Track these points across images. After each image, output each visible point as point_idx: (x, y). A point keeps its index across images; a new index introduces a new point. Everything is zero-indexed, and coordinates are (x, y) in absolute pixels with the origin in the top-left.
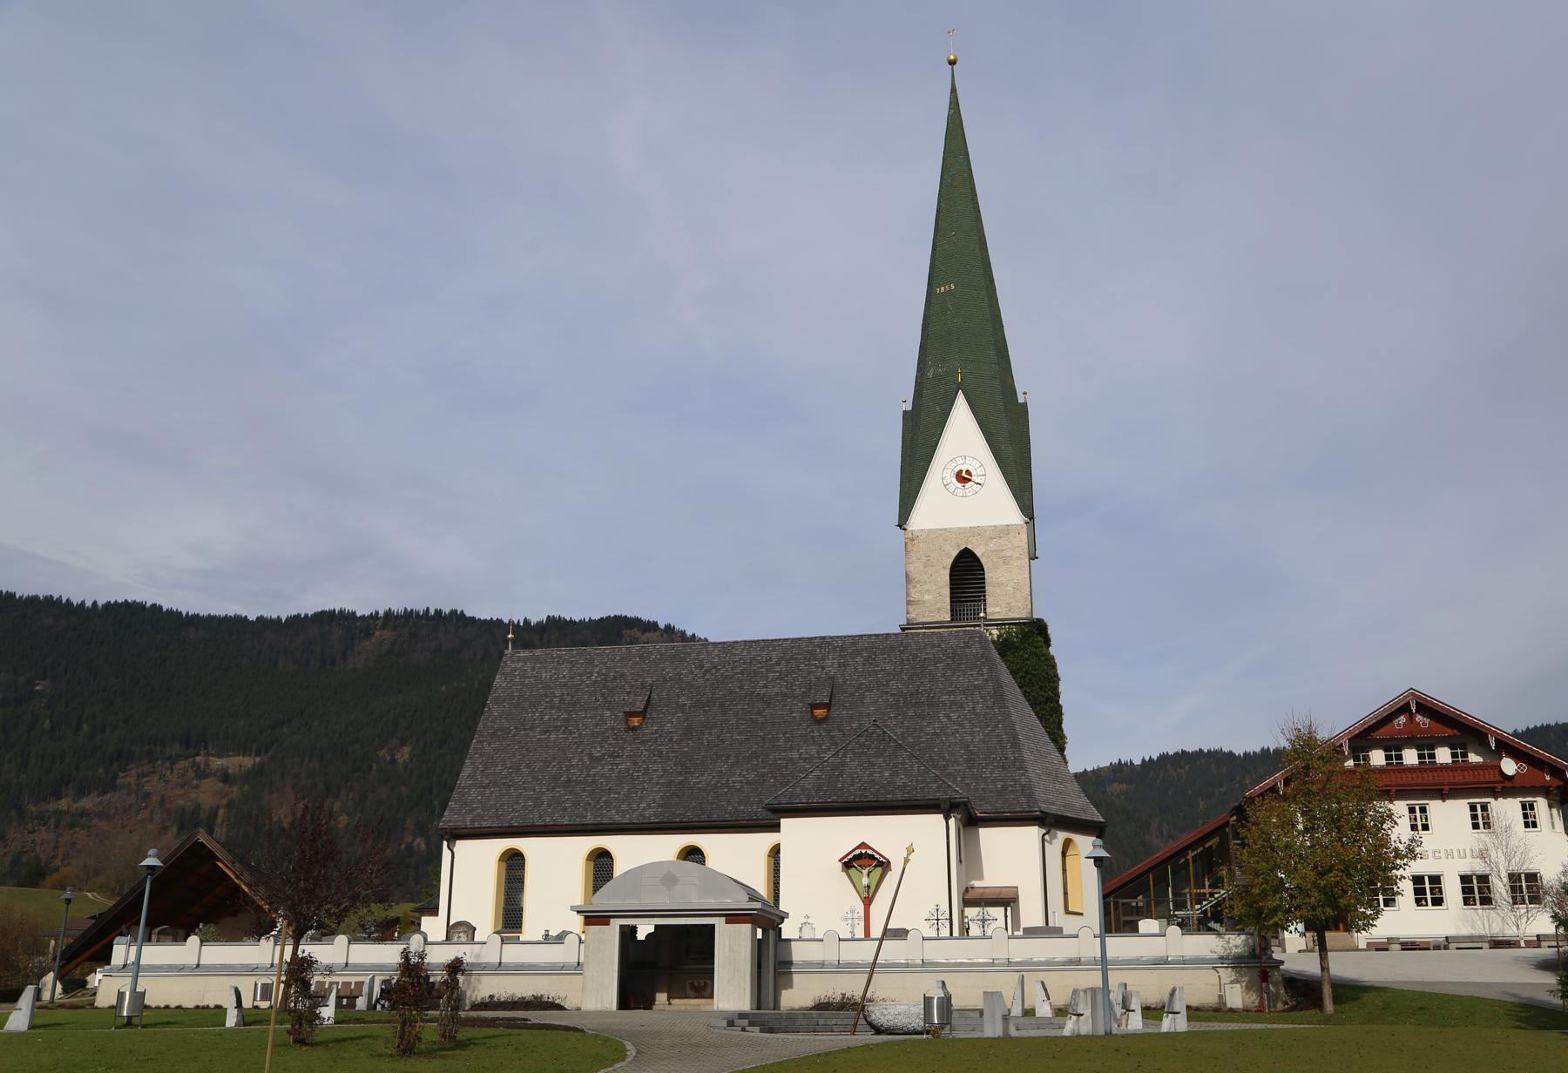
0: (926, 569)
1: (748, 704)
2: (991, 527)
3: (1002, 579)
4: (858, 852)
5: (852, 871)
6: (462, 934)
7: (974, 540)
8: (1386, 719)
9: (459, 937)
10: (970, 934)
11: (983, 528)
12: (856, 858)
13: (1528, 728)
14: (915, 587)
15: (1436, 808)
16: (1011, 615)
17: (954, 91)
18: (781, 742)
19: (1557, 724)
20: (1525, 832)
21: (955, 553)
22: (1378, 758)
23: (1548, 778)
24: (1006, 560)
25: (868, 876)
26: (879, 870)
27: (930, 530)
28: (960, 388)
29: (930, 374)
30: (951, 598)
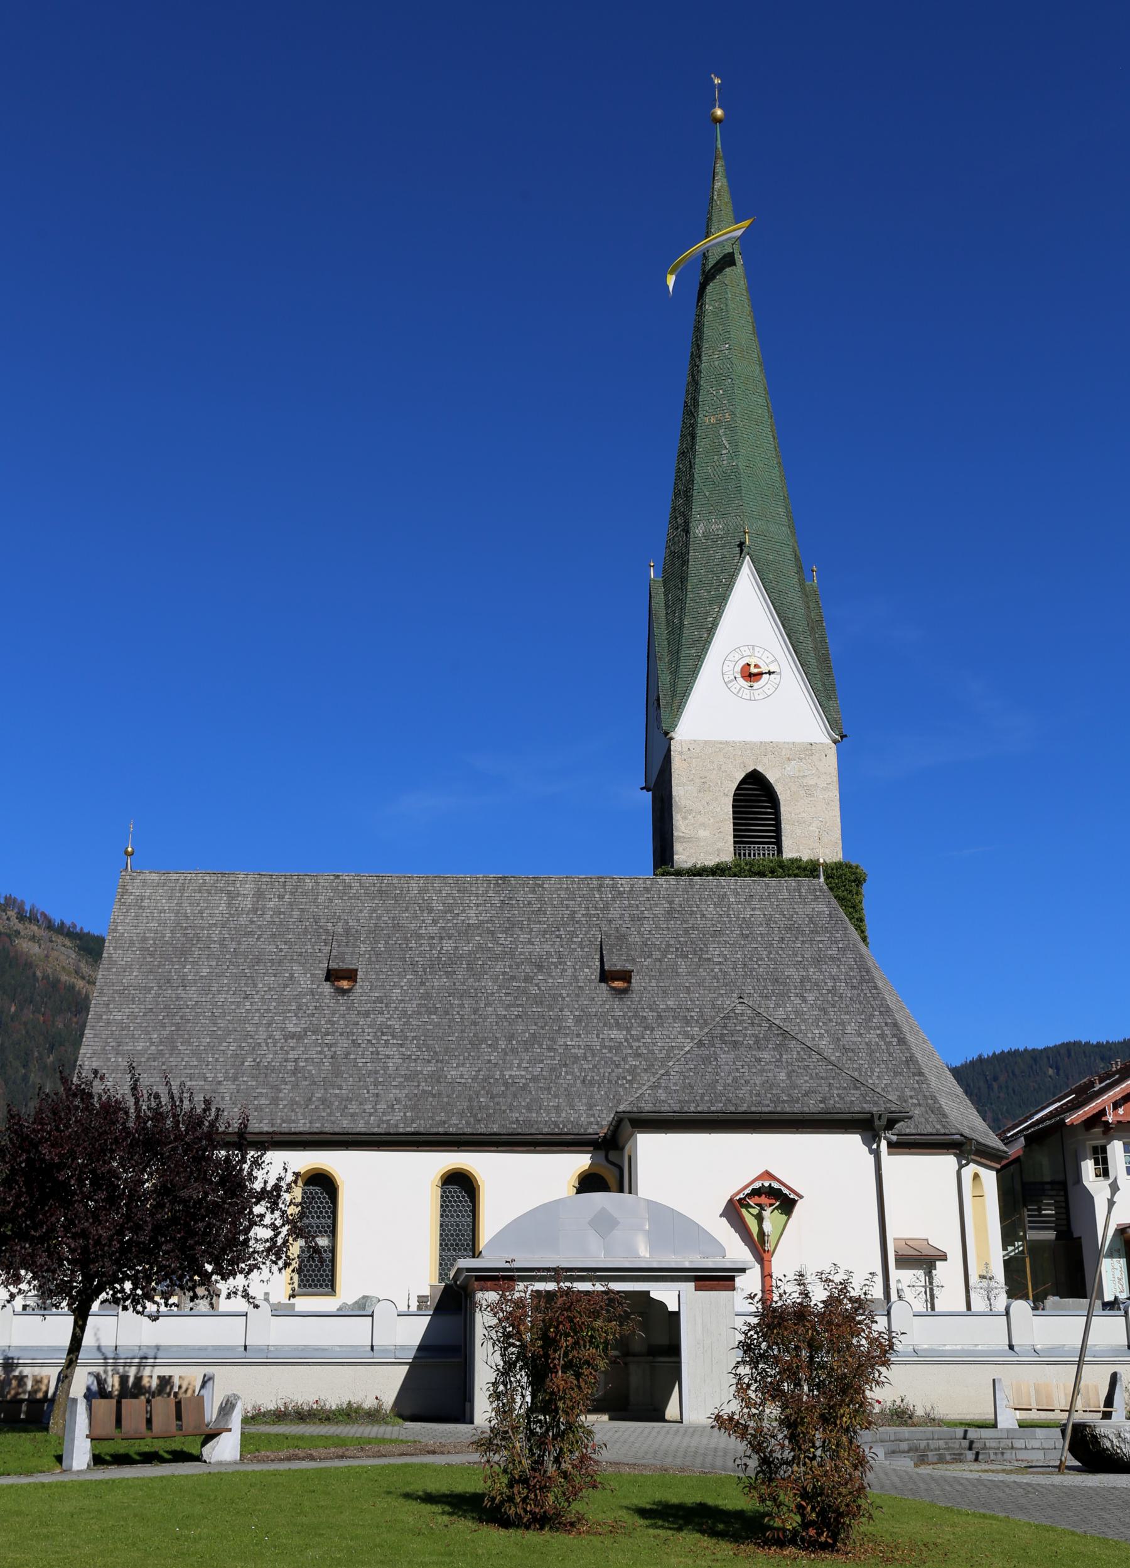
0: (701, 795)
1: (510, 967)
2: (788, 743)
4: (758, 1185)
7: (765, 760)
10: (937, 1309)
11: (778, 744)
13: (994, 1053)
14: (685, 818)
18: (570, 1023)
19: (1026, 1050)
20: (801, 1197)
21: (740, 776)
27: (706, 742)
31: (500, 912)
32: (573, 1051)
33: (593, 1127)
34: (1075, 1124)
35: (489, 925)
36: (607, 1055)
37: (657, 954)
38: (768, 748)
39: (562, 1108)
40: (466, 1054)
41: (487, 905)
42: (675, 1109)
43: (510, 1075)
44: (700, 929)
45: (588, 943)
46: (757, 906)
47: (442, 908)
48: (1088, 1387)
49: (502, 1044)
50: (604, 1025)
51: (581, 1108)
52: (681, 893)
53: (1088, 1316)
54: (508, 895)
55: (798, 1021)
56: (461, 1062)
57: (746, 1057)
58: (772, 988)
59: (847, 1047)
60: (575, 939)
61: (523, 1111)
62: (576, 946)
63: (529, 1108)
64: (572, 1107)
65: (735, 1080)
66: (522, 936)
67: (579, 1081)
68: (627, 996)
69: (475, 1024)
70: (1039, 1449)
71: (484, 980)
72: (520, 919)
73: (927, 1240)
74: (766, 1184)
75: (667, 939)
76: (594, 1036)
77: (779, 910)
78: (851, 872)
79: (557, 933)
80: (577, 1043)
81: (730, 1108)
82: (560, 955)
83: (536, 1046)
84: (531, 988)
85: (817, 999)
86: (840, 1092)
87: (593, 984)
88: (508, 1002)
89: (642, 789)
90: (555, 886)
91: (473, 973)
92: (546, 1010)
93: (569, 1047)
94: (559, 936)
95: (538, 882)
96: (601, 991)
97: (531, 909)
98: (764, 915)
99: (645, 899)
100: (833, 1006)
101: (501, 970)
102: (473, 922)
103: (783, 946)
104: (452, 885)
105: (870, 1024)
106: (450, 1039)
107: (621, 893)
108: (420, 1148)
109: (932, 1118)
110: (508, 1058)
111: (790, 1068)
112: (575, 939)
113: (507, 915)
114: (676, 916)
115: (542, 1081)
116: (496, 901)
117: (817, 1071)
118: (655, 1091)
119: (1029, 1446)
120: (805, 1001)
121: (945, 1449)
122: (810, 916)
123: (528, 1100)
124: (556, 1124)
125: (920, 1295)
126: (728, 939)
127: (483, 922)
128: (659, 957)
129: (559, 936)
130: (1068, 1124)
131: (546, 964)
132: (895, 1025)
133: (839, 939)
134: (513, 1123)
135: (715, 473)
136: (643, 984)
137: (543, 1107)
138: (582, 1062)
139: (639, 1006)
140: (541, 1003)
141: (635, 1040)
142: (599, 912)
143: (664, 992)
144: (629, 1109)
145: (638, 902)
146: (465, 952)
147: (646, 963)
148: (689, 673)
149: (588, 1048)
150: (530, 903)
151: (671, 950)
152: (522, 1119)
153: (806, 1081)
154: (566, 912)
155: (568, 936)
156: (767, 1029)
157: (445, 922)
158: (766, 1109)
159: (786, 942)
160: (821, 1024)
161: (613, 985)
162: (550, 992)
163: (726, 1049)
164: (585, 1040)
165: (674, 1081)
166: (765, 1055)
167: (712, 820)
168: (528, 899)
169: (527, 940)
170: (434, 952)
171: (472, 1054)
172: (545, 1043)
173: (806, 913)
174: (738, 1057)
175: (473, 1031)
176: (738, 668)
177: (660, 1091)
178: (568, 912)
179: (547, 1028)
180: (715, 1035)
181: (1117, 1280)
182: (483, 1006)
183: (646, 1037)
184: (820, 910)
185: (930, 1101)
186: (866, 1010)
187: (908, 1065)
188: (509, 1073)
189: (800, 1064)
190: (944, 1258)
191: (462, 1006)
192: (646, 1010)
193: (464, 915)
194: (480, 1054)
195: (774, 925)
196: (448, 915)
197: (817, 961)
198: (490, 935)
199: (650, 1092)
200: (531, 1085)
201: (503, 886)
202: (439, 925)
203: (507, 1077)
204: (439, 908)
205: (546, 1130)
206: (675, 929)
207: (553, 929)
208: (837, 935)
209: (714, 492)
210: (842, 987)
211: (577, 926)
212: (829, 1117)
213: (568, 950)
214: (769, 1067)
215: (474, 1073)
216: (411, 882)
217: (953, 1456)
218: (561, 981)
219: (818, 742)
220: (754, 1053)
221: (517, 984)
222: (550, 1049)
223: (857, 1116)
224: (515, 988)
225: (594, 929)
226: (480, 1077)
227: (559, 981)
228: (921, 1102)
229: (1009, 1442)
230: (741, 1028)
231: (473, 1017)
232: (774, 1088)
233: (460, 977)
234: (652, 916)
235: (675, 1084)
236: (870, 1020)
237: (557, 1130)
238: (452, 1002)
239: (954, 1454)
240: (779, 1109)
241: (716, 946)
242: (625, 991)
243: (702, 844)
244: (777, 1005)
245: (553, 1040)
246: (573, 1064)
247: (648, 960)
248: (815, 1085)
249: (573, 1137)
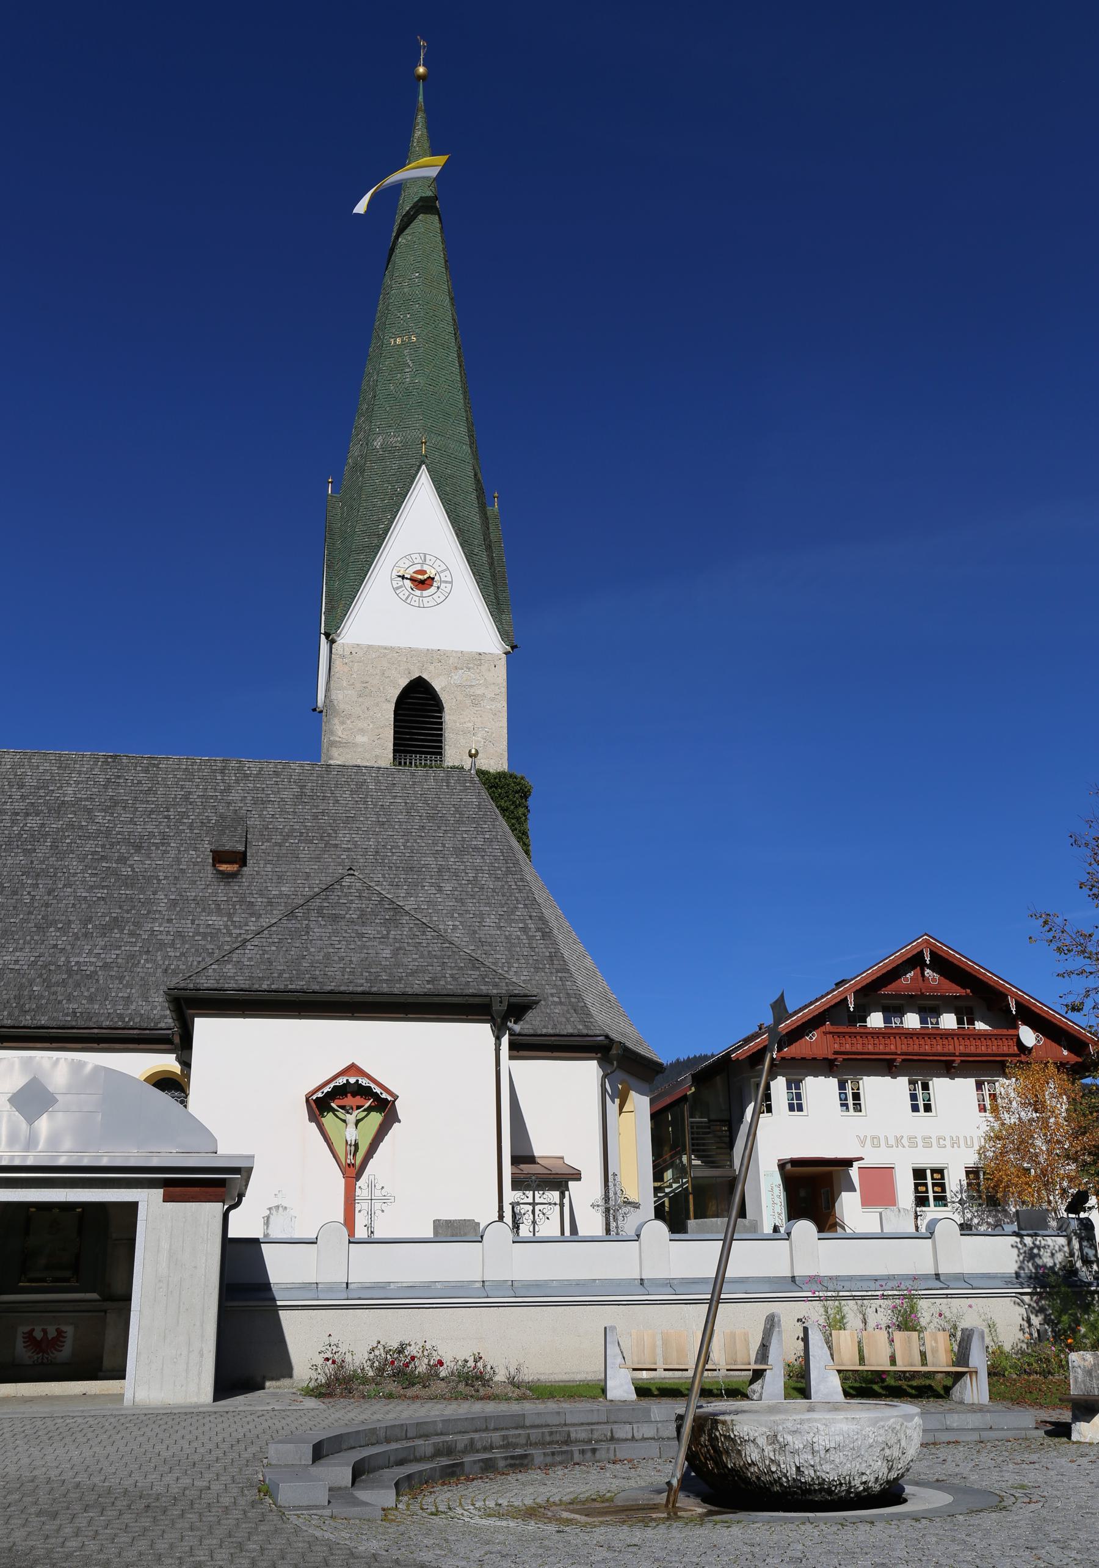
0: (360, 700)
1: (103, 846)
2: (456, 652)
4: (341, 1081)
5: (329, 1120)
8: (893, 974)
12: (339, 1092)
14: (343, 723)
15: (940, 1086)
18: (162, 907)
21: (404, 682)
22: (876, 1020)
23: (1065, 1053)
25: (356, 1125)
26: (376, 1118)
27: (369, 647)
28: (423, 462)
29: (377, 444)
31: (104, 790)
32: (159, 937)
33: (166, 1020)
34: (740, 1059)
35: (87, 803)
36: (200, 942)
37: (278, 838)
38: (436, 656)
39: (133, 999)
40: (28, 938)
41: (90, 783)
42: (243, 986)
43: (77, 963)
44: (331, 815)
45: (199, 824)
46: (398, 794)
47: (36, 784)
48: (735, 1335)
49: (75, 927)
50: (204, 910)
51: (157, 1000)
52: (315, 778)
53: (724, 1240)
54: (116, 774)
55: (430, 911)
56: (20, 946)
57: (346, 932)
58: (404, 876)
59: (483, 940)
60: (185, 821)
61: (84, 1002)
62: (184, 828)
63: (91, 999)
64: (146, 999)
65: (327, 956)
66: (123, 815)
67: (159, 970)
68: (235, 880)
69: (47, 905)
70: (653, 1439)
71: (69, 859)
72: (125, 798)
73: (563, 1158)
74: (352, 1080)
75: (292, 824)
76: (189, 922)
77: (423, 799)
78: (515, 783)
79: (166, 813)
80: (167, 929)
81: (313, 987)
82: (164, 836)
83: (116, 931)
84: (123, 870)
85: (455, 889)
86: (455, 972)
87: (197, 867)
88: (93, 883)
90: (172, 766)
91: (57, 851)
92: (136, 892)
93: (155, 933)
94: (168, 817)
95: (153, 762)
96: (205, 875)
97: (140, 789)
98: (406, 803)
99: (273, 783)
100: (473, 897)
101: (91, 849)
102: (69, 799)
103: (423, 834)
104: (53, 761)
105: (512, 917)
106: (12, 920)
107: (246, 776)
108: (469, 1017)
109: (574, 1018)
110: (79, 943)
111: (397, 945)
112: (185, 821)
113: (110, 794)
114: (306, 800)
115: (115, 969)
116: (101, 779)
117: (430, 949)
118: (222, 967)
119: (638, 1436)
120: (440, 889)
121: (502, 1447)
122: (457, 806)
123: (93, 990)
124: (121, 1017)
125: (526, 1216)
126: (362, 826)
127: (81, 800)
128: (280, 841)
129: (168, 817)
130: (733, 1059)
131: (146, 844)
132: (542, 918)
133: (486, 830)
134: (67, 1015)
136: (256, 869)
137: (110, 998)
138: (169, 950)
139: (247, 892)
140: (132, 886)
141: (235, 927)
142: (217, 794)
143: (280, 877)
144: (182, 985)
145: (265, 786)
146: (52, 830)
147: (263, 847)
149: (179, 934)
150: (140, 782)
151: (294, 834)
152: (80, 1010)
153: (414, 960)
154: (180, 793)
155: (177, 817)
156: (377, 902)
157: (36, 798)
158: (360, 989)
159: (426, 831)
160: (456, 915)
161: (221, 869)
162: (145, 874)
163: (323, 923)
164: (177, 925)
165: (250, 956)
166: (370, 931)
167: (371, 726)
168: (138, 779)
169: (129, 819)
170: (15, 828)
171: (35, 938)
172: (127, 928)
173: (453, 803)
174: (335, 933)
175: (42, 913)
177: (230, 966)
178: (183, 793)
179: (133, 912)
180: (312, 908)
181: (777, 1215)
182: (61, 886)
183: (251, 924)
184: (468, 800)
185: (573, 1000)
186: (509, 902)
187: (552, 960)
188: (77, 959)
189: (410, 941)
190: (578, 1177)
191: (35, 886)
192: (255, 896)
193: (60, 792)
194: (45, 938)
195: (415, 814)
196: (41, 791)
197: (459, 852)
198: (86, 813)
199: (216, 967)
200: (100, 973)
201: (112, 764)
202: (27, 801)
203: (73, 964)
204: (32, 784)
205: (107, 1023)
206: (302, 814)
207: (162, 809)
208: (484, 826)
209: (394, 407)
210: (484, 879)
211: (190, 807)
212: (436, 1000)
213: (175, 831)
214: (372, 944)
215: (32, 959)
216: (6, 756)
217: (510, 1461)
218: (161, 862)
220: (356, 928)
221: (107, 865)
222: (132, 934)
223: (472, 1000)
224: (104, 869)
225: (209, 811)
226: (39, 963)
227: (159, 862)
228: (563, 1000)
229: (606, 1429)
230: (346, 901)
231: (46, 898)
232: (374, 966)
233: (40, 855)
234: (278, 800)
235: (250, 959)
236: (513, 913)
237: (120, 1023)
238: (25, 881)
239: (512, 1457)
240: (374, 989)
241: (346, 832)
242: (233, 875)
243: (360, 750)
244: (409, 894)
245: (137, 924)
246: (157, 951)
247: (265, 844)
248: (426, 964)
249: (135, 1032)
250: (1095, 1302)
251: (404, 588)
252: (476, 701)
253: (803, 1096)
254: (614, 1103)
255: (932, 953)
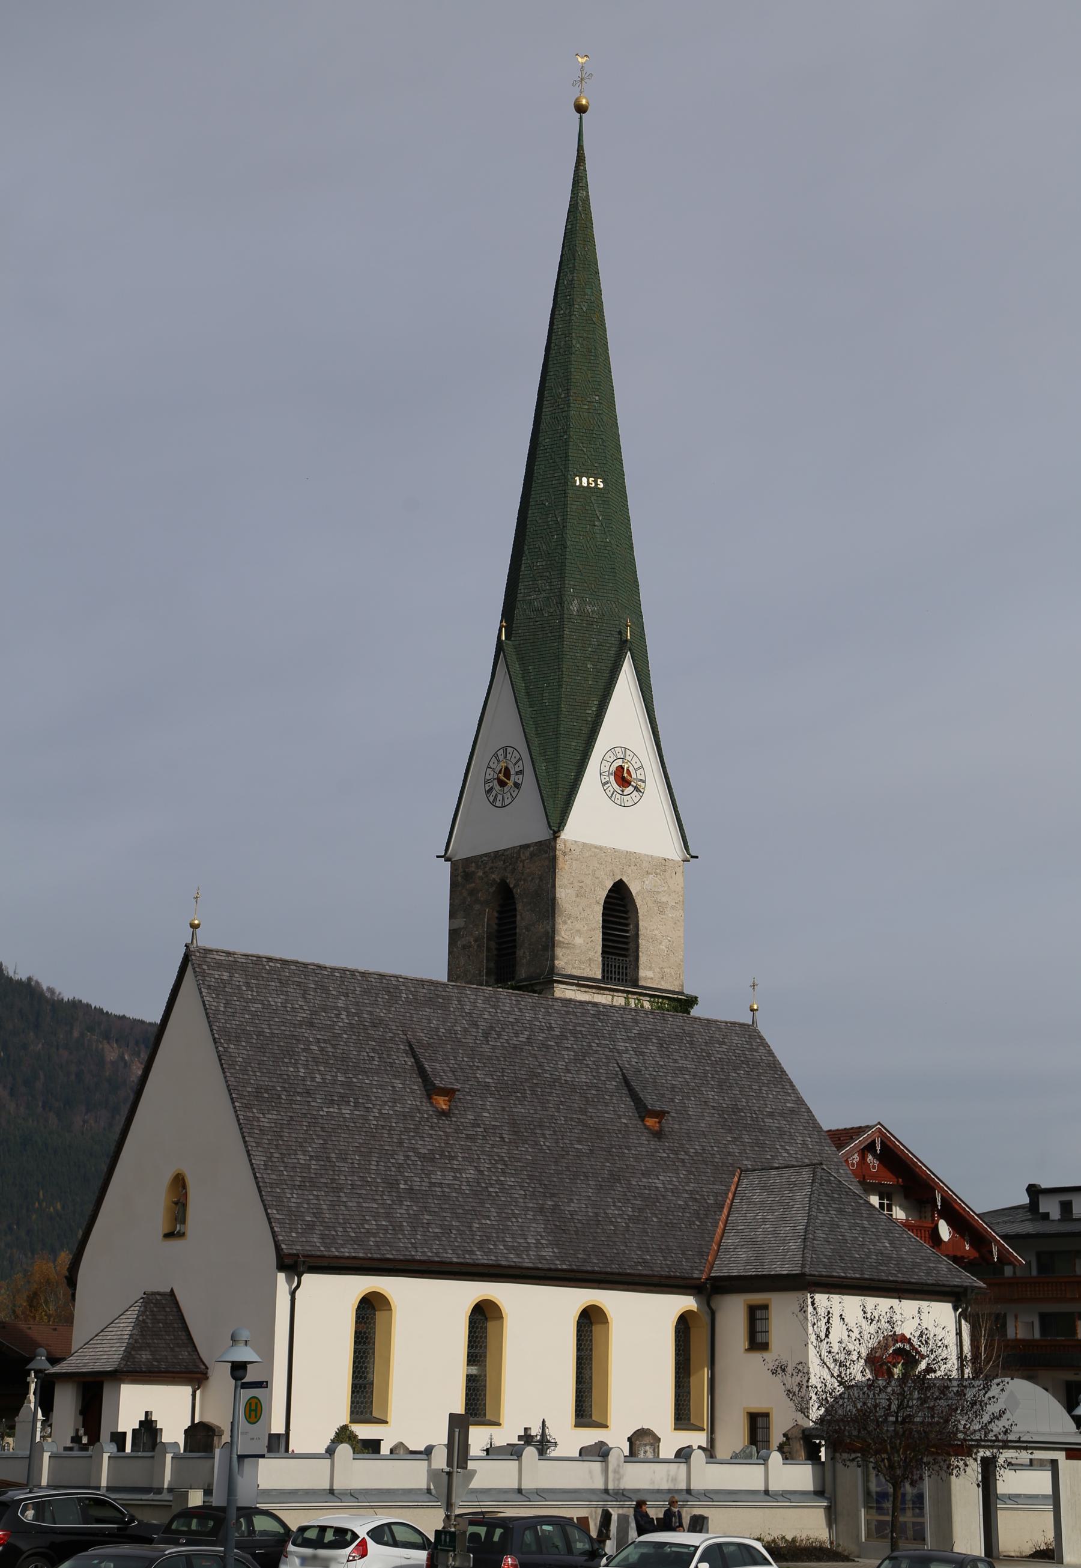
0: (578, 900)
2: (648, 856)
3: (657, 932)
6: (648, 1448)
9: (645, 1452)
16: (664, 985)
17: (580, 159)
21: (609, 885)
24: (662, 908)
30: (603, 946)
38: (631, 859)
89: (438, 857)
135: (588, 546)
148: (571, 767)
167: (586, 928)
176: (613, 768)
219: (670, 858)
250: (36, 1380)
251: (609, 784)
252: (662, 908)
253: (233, 1113)
254: (511, 1455)
255: (882, 1143)
